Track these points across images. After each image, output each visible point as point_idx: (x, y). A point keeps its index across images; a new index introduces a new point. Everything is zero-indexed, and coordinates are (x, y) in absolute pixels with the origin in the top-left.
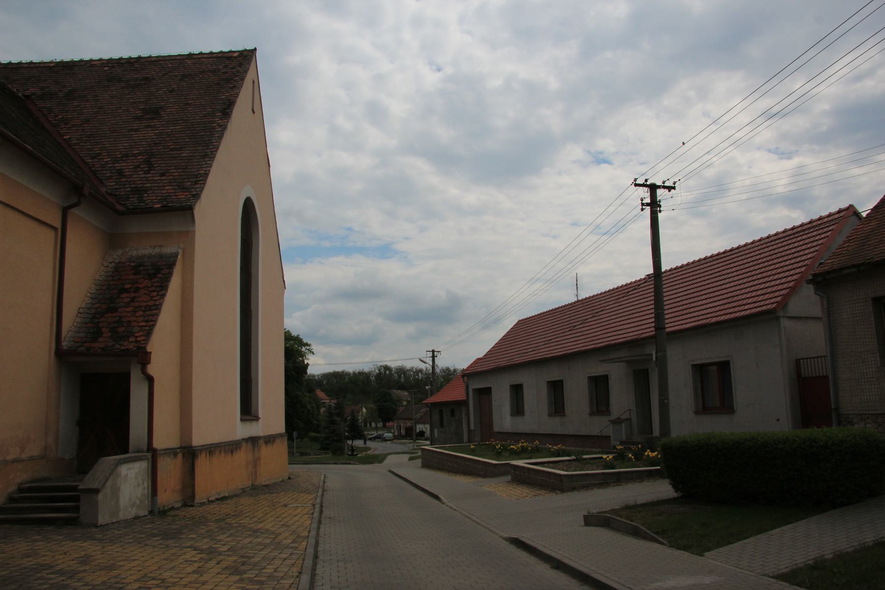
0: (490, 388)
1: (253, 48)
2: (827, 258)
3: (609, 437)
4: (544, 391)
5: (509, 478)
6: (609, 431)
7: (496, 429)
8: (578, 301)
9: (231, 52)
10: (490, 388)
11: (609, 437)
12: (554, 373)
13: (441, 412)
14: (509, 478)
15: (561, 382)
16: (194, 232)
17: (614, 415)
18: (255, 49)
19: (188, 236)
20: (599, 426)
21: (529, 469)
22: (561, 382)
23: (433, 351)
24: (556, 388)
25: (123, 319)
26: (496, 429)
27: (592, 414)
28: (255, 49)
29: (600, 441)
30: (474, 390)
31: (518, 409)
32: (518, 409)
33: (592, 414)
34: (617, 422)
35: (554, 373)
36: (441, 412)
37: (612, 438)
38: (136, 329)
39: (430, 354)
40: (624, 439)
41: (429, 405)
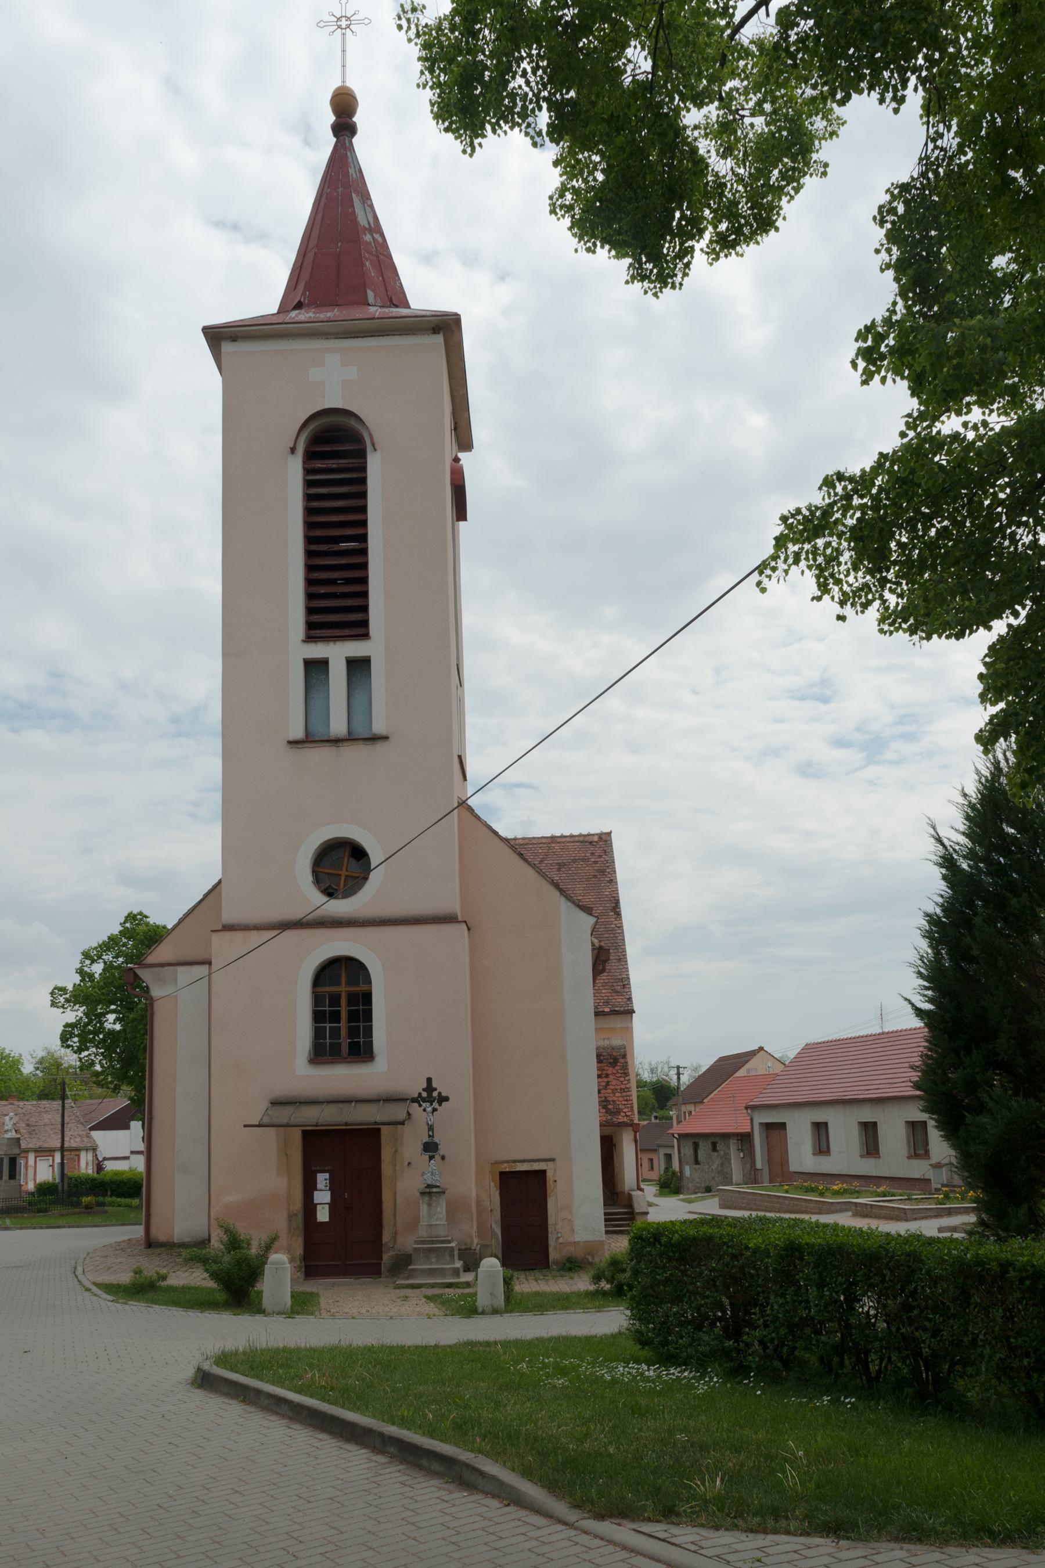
0: (785, 1124)
1: (609, 831)
2: (591, 1551)
3: (930, 1180)
4: (855, 1133)
5: (850, 1213)
6: (930, 1175)
7: (793, 1167)
8: (883, 1033)
9: (589, 835)
10: (785, 1124)
11: (930, 1180)
12: (867, 1115)
13: (696, 1146)
14: (850, 1213)
15: (874, 1125)
16: (632, 1028)
17: (934, 1160)
18: (611, 832)
19: (628, 1030)
20: (918, 1169)
21: (872, 1205)
22: (874, 1125)
23: (678, 1067)
24: (869, 1130)
25: (609, 1099)
26: (793, 1167)
27: (910, 1157)
28: (611, 832)
29: (923, 1183)
30: (761, 1124)
31: (822, 1147)
32: (822, 1147)
33: (910, 1157)
34: (938, 1166)
35: (867, 1115)
36: (696, 1146)
37: (932, 1182)
38: (621, 1107)
39: (675, 1071)
40: (945, 1182)
41: (676, 1136)
